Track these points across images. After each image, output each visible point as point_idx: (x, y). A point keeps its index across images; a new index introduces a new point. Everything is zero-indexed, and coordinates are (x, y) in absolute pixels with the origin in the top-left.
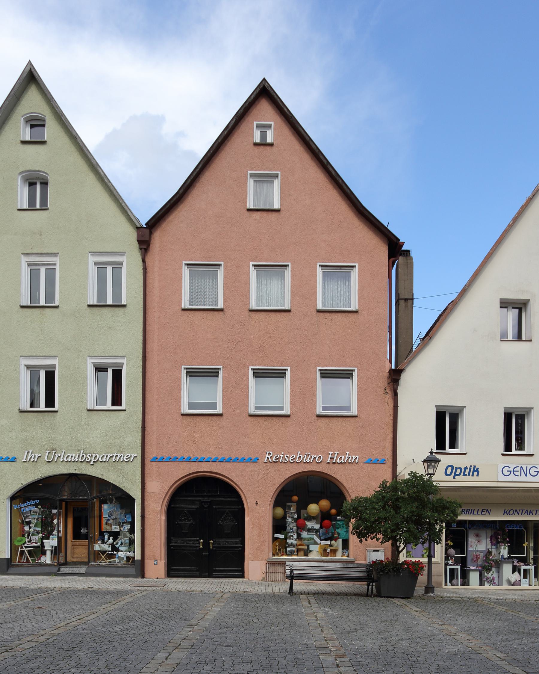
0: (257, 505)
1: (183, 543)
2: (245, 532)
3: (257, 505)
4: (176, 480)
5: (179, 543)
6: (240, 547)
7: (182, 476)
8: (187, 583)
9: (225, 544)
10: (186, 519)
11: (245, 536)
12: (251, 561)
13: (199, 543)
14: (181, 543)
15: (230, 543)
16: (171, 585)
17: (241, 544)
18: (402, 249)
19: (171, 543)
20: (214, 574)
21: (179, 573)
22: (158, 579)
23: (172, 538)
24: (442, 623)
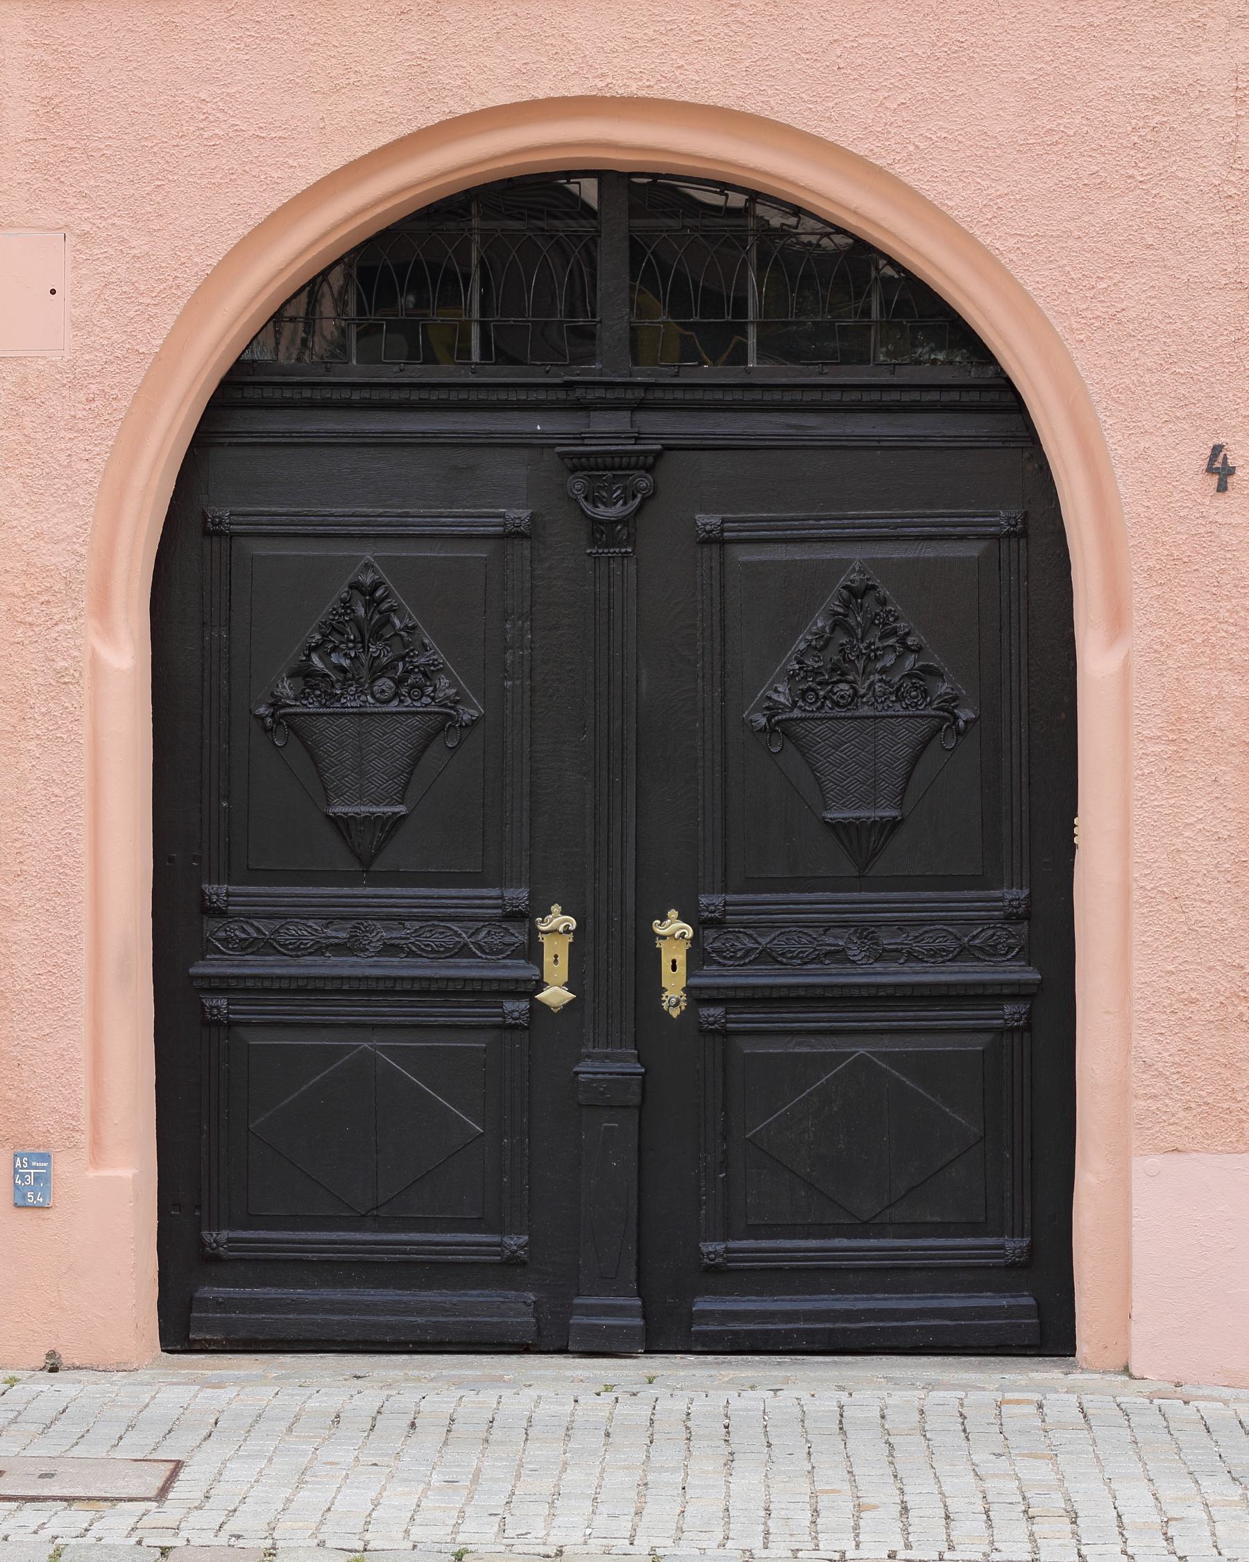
0: (1222, 488)
1: (340, 948)
2: (1071, 808)
3: (1222, 488)
4: (259, 214)
5: (298, 949)
6: (1018, 993)
7: (336, 163)
8: (429, 1438)
9: (839, 955)
10: (378, 671)
11: (1073, 847)
12: (1156, 1161)
13: (533, 952)
14: (319, 950)
15: (887, 941)
16: (241, 1472)
17: (1027, 954)
18: (597, 208)
19: (204, 949)
20: (705, 1314)
21: (296, 1306)
22: (64, 1388)
23: (216, 891)
24: (767, 1382)
